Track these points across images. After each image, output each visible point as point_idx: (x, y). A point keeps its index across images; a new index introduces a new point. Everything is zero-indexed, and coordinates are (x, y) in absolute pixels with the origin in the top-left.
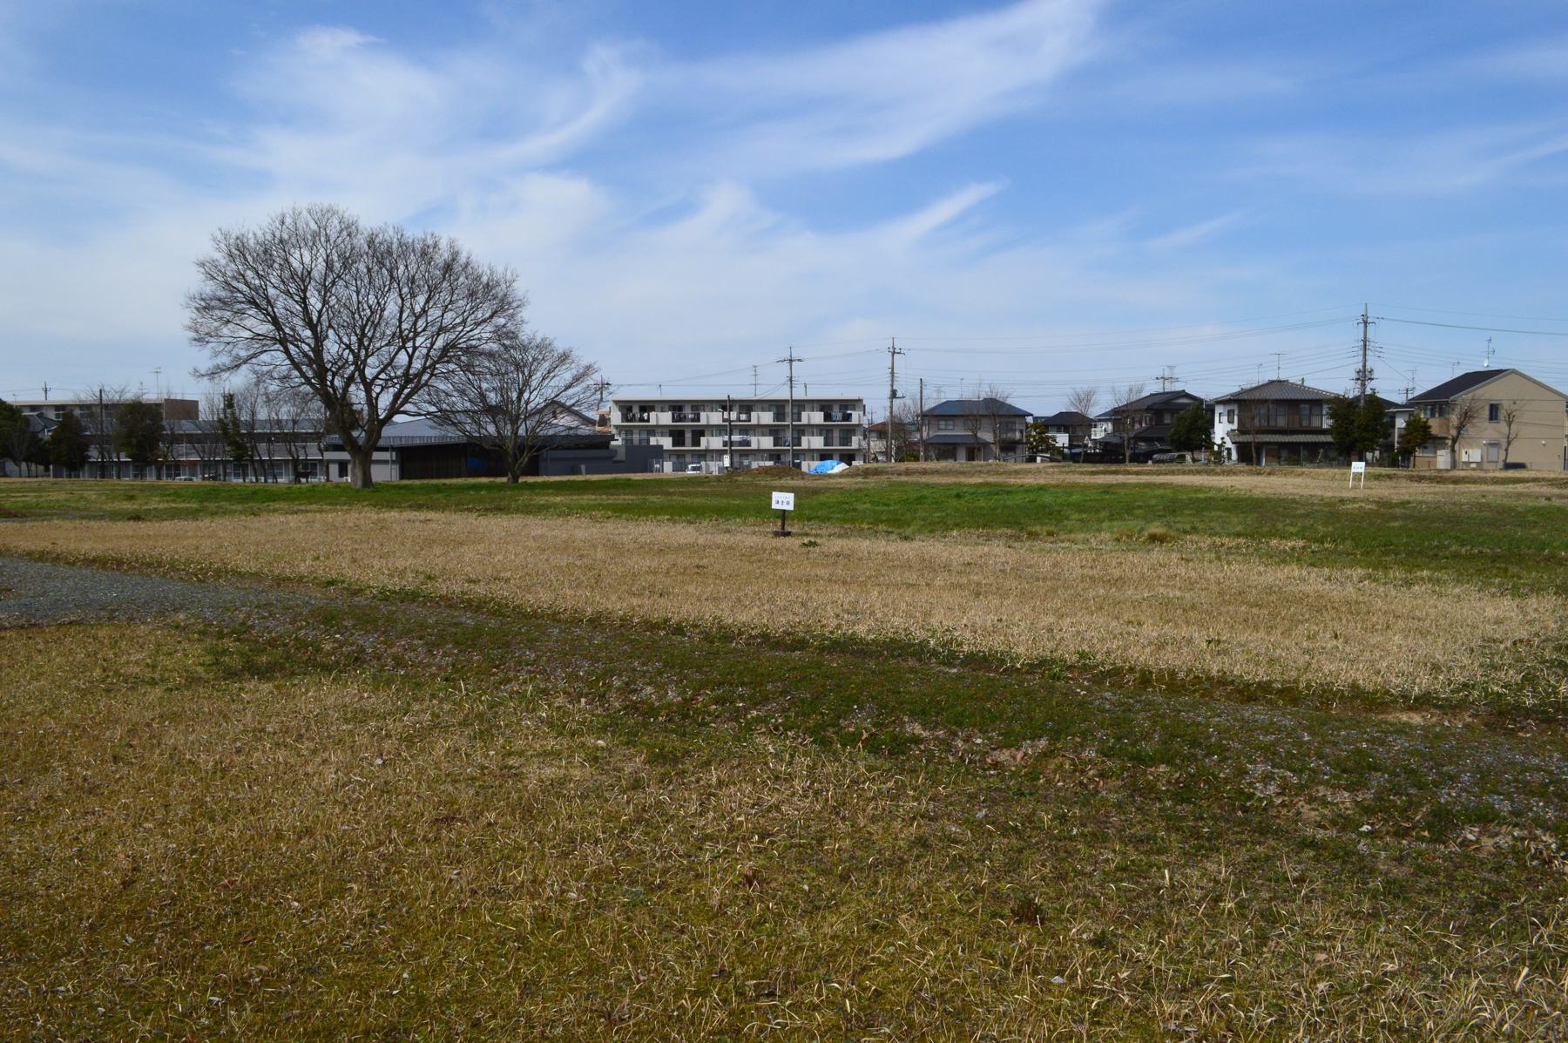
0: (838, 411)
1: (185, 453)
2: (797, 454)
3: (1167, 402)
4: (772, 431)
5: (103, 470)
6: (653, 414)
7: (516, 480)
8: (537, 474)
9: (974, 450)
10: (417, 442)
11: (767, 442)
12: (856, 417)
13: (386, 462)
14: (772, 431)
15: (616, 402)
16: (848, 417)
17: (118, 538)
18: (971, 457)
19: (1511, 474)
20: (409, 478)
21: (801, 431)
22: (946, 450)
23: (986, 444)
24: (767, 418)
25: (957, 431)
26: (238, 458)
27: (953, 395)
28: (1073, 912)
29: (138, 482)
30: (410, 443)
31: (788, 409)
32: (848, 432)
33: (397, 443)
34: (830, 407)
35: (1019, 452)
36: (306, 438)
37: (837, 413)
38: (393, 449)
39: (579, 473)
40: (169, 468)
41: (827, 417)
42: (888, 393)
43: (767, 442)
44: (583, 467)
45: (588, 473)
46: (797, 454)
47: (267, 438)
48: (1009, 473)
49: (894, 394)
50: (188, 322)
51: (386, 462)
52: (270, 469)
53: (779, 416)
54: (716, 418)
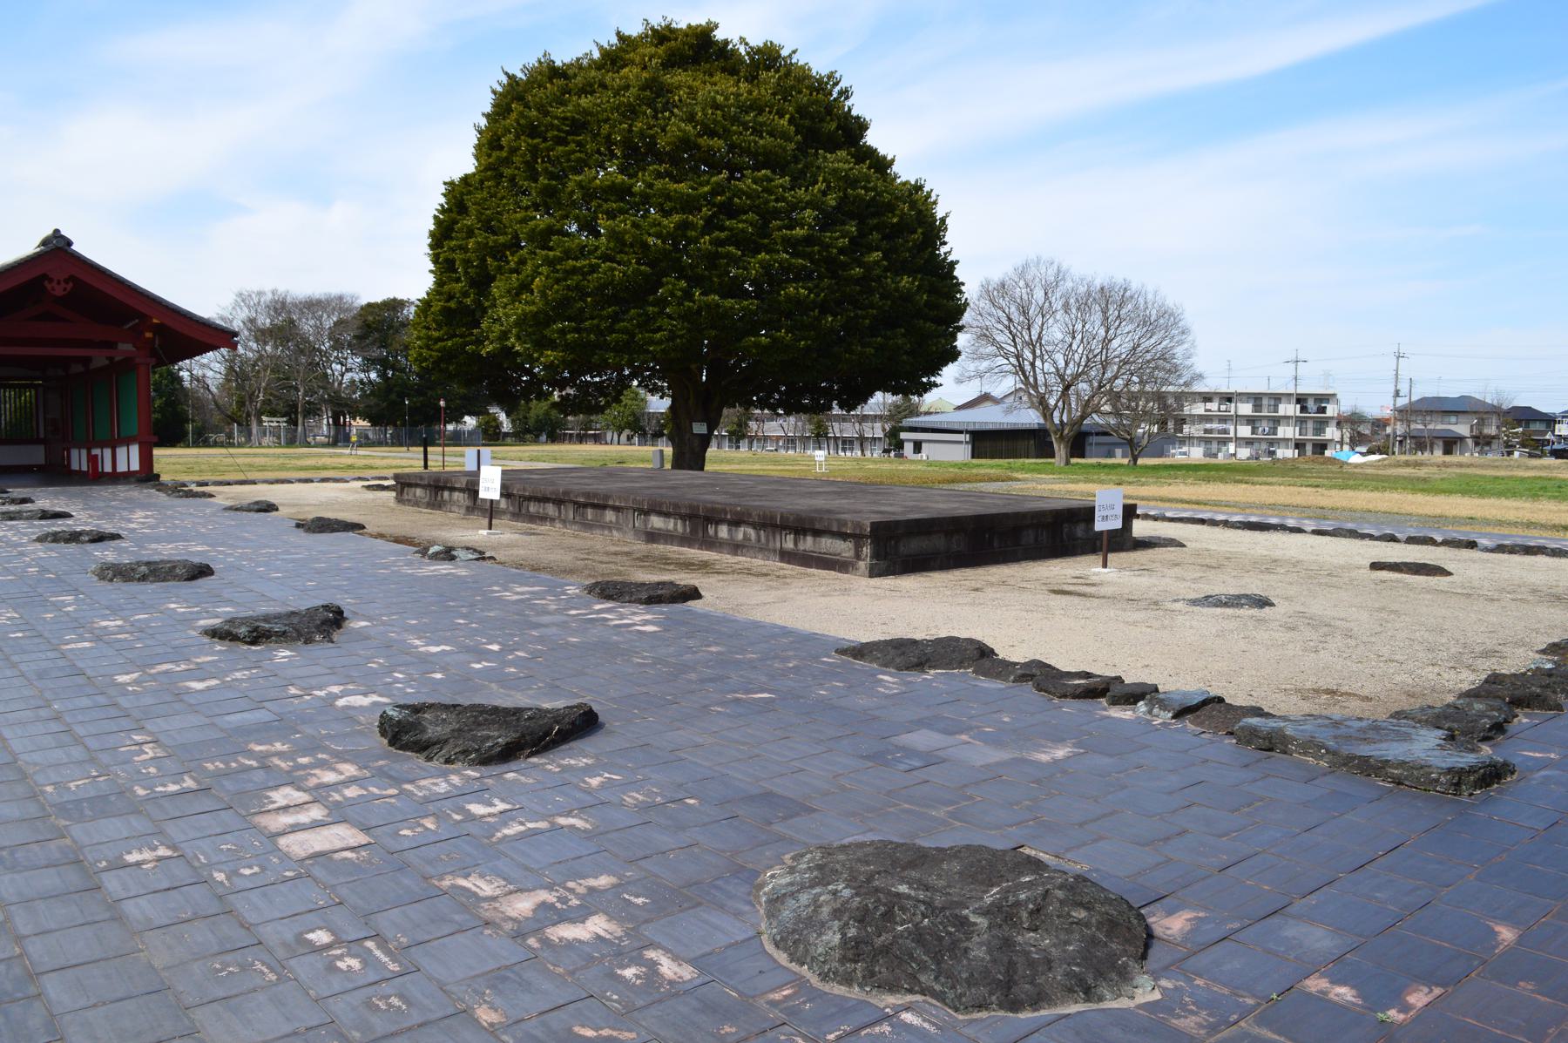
0: (1313, 405)
2: (1272, 443)
4: (1250, 421)
7: (1135, 460)
9: (1451, 444)
10: (990, 427)
11: (1245, 431)
12: (1331, 411)
14: (1250, 421)
16: (1323, 410)
18: (1448, 451)
19: (1254, 587)
20: (979, 457)
21: (1277, 421)
22: (1421, 443)
23: (1462, 439)
24: (1246, 409)
25: (1438, 426)
26: (818, 435)
27: (1431, 392)
30: (984, 428)
31: (1265, 402)
32: (1321, 424)
33: (971, 428)
34: (1305, 400)
35: (1494, 446)
37: (1311, 404)
40: (844, 442)
41: (1303, 409)
42: (1392, 389)
43: (1245, 431)
46: (1272, 443)
48: (279, 456)
49: (1397, 394)
53: (1257, 407)
54: (1199, 409)
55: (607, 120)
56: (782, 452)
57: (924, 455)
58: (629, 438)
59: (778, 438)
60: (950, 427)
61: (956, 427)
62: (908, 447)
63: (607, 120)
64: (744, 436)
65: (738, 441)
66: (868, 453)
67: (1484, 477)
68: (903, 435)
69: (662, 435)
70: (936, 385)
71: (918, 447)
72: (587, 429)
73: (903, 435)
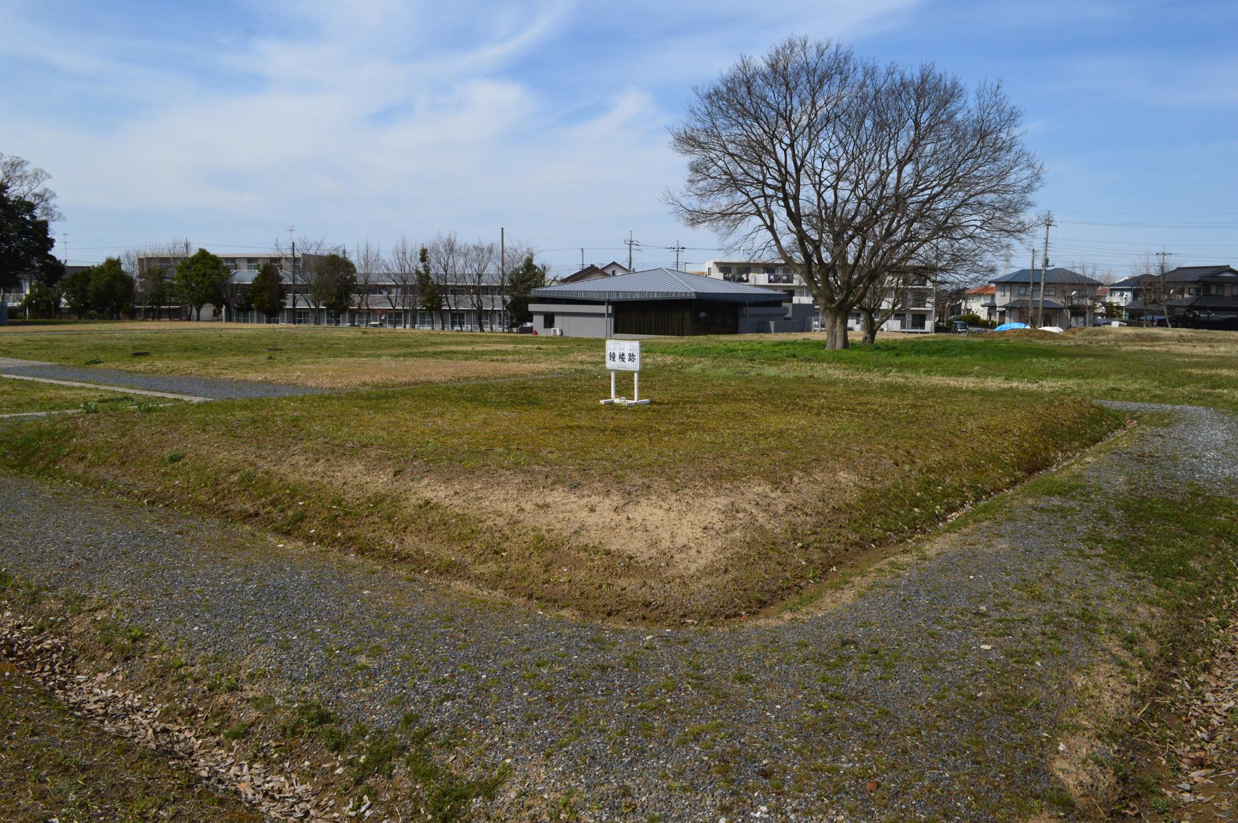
1: (379, 302)
3: (1213, 276)
5: (297, 316)
6: (751, 275)
8: (735, 330)
13: (602, 315)
15: (717, 264)
17: (938, 380)
28: (1149, 569)
29: (1130, 331)
30: (629, 298)
33: (614, 298)
36: (487, 290)
38: (610, 303)
39: (768, 331)
44: (772, 324)
45: (777, 330)
47: (456, 290)
50: (908, 76)
51: (602, 315)
52: (458, 317)
55: (659, 708)
56: (389, 327)
57: (556, 330)
58: (216, 313)
59: (384, 311)
60: (588, 297)
61: (596, 297)
62: (538, 322)
63: (659, 708)
64: (344, 310)
65: (337, 316)
66: (487, 329)
67: (795, 343)
68: (532, 307)
69: (251, 309)
70: (1029, 204)
71: (549, 320)
72: (159, 304)
73: (532, 307)
